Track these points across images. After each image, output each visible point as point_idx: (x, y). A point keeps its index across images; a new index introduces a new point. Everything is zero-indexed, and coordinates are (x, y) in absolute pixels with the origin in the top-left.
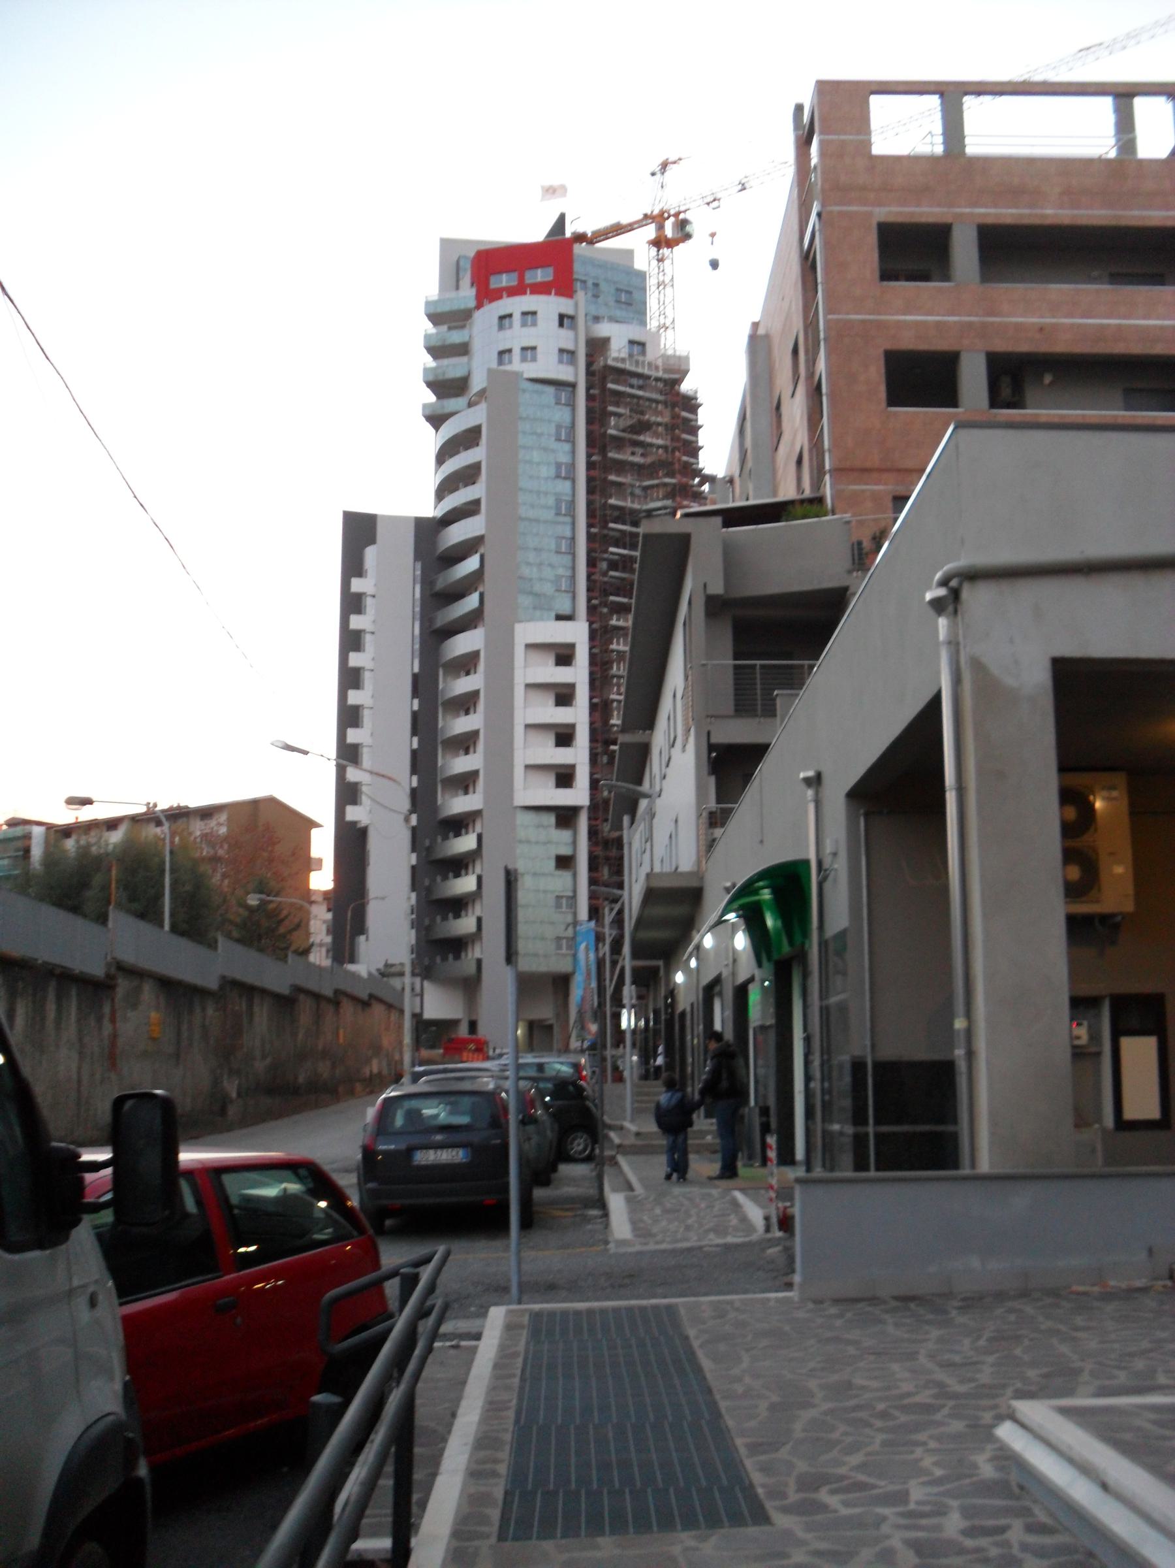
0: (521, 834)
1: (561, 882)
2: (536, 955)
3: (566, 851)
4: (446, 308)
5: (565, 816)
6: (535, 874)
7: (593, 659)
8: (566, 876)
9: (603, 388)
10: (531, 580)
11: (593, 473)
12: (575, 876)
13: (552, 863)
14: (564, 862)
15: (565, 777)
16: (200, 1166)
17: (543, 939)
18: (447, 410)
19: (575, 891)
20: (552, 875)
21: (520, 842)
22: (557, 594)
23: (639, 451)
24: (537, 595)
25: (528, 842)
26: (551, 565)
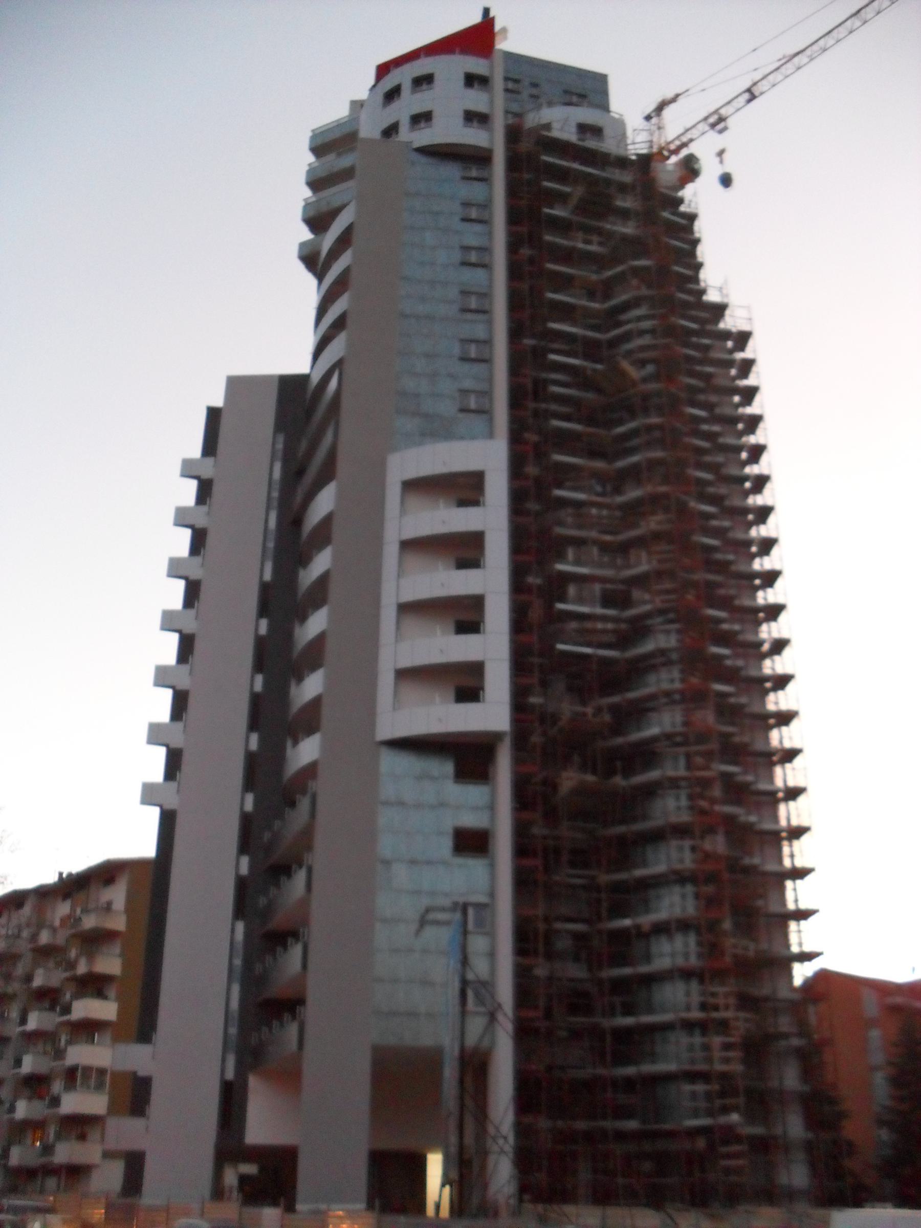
0: (388, 790)
1: (468, 878)
2: (412, 1014)
3: (471, 820)
4: (322, 174)
5: (469, 756)
6: (413, 862)
7: (520, 623)
8: (475, 867)
9: (548, 650)
10: (417, 395)
11: (528, 862)
12: (492, 866)
13: (447, 844)
14: (472, 842)
15: (466, 684)
16: (335, 124)
17: (426, 983)
18: (336, 203)
19: (492, 894)
20: (444, 863)
21: (386, 803)
22: (461, 415)
23: (595, 238)
24: (426, 416)
25: (401, 804)
26: (451, 376)
